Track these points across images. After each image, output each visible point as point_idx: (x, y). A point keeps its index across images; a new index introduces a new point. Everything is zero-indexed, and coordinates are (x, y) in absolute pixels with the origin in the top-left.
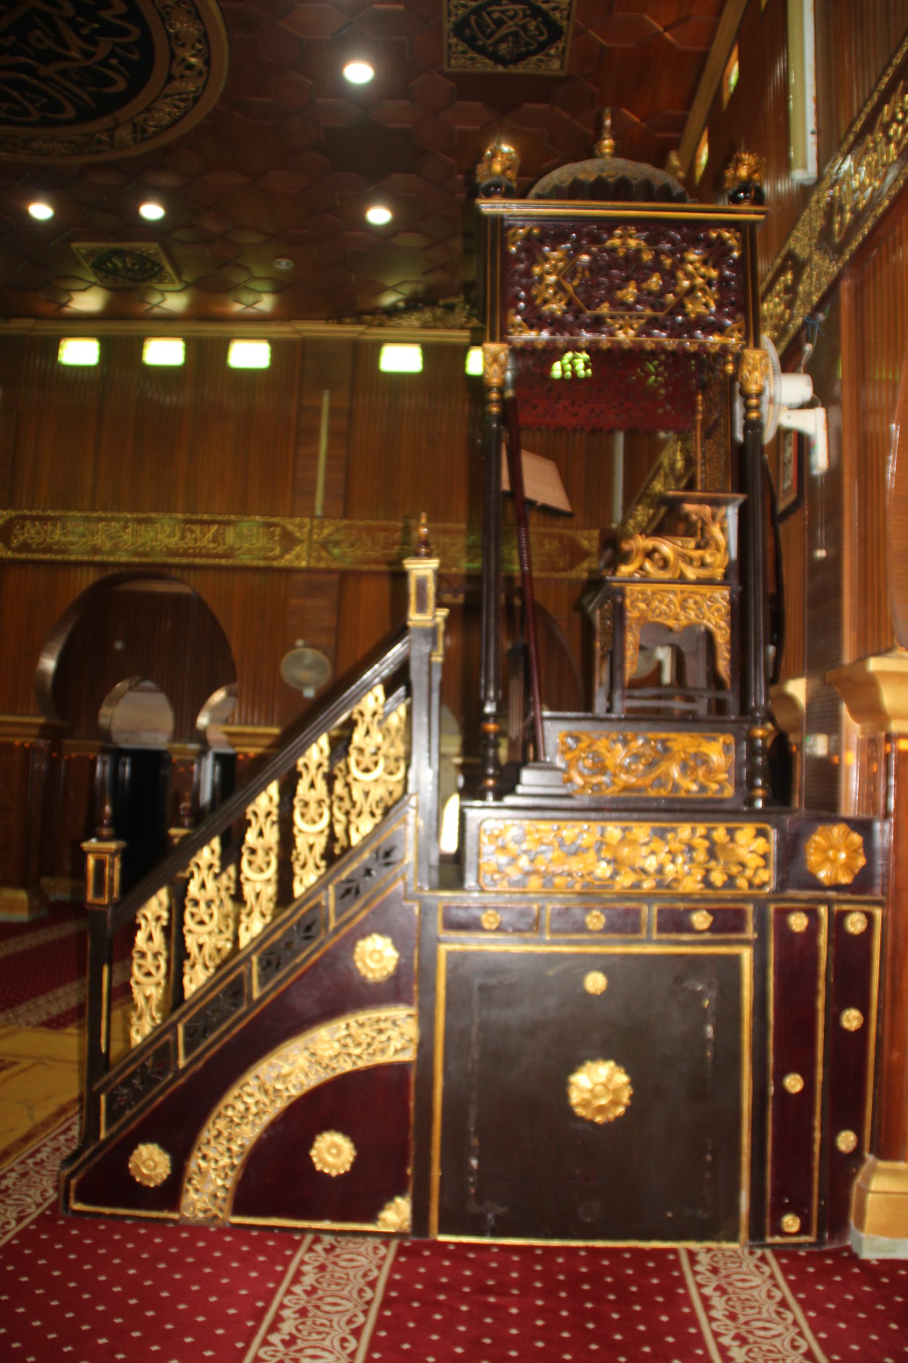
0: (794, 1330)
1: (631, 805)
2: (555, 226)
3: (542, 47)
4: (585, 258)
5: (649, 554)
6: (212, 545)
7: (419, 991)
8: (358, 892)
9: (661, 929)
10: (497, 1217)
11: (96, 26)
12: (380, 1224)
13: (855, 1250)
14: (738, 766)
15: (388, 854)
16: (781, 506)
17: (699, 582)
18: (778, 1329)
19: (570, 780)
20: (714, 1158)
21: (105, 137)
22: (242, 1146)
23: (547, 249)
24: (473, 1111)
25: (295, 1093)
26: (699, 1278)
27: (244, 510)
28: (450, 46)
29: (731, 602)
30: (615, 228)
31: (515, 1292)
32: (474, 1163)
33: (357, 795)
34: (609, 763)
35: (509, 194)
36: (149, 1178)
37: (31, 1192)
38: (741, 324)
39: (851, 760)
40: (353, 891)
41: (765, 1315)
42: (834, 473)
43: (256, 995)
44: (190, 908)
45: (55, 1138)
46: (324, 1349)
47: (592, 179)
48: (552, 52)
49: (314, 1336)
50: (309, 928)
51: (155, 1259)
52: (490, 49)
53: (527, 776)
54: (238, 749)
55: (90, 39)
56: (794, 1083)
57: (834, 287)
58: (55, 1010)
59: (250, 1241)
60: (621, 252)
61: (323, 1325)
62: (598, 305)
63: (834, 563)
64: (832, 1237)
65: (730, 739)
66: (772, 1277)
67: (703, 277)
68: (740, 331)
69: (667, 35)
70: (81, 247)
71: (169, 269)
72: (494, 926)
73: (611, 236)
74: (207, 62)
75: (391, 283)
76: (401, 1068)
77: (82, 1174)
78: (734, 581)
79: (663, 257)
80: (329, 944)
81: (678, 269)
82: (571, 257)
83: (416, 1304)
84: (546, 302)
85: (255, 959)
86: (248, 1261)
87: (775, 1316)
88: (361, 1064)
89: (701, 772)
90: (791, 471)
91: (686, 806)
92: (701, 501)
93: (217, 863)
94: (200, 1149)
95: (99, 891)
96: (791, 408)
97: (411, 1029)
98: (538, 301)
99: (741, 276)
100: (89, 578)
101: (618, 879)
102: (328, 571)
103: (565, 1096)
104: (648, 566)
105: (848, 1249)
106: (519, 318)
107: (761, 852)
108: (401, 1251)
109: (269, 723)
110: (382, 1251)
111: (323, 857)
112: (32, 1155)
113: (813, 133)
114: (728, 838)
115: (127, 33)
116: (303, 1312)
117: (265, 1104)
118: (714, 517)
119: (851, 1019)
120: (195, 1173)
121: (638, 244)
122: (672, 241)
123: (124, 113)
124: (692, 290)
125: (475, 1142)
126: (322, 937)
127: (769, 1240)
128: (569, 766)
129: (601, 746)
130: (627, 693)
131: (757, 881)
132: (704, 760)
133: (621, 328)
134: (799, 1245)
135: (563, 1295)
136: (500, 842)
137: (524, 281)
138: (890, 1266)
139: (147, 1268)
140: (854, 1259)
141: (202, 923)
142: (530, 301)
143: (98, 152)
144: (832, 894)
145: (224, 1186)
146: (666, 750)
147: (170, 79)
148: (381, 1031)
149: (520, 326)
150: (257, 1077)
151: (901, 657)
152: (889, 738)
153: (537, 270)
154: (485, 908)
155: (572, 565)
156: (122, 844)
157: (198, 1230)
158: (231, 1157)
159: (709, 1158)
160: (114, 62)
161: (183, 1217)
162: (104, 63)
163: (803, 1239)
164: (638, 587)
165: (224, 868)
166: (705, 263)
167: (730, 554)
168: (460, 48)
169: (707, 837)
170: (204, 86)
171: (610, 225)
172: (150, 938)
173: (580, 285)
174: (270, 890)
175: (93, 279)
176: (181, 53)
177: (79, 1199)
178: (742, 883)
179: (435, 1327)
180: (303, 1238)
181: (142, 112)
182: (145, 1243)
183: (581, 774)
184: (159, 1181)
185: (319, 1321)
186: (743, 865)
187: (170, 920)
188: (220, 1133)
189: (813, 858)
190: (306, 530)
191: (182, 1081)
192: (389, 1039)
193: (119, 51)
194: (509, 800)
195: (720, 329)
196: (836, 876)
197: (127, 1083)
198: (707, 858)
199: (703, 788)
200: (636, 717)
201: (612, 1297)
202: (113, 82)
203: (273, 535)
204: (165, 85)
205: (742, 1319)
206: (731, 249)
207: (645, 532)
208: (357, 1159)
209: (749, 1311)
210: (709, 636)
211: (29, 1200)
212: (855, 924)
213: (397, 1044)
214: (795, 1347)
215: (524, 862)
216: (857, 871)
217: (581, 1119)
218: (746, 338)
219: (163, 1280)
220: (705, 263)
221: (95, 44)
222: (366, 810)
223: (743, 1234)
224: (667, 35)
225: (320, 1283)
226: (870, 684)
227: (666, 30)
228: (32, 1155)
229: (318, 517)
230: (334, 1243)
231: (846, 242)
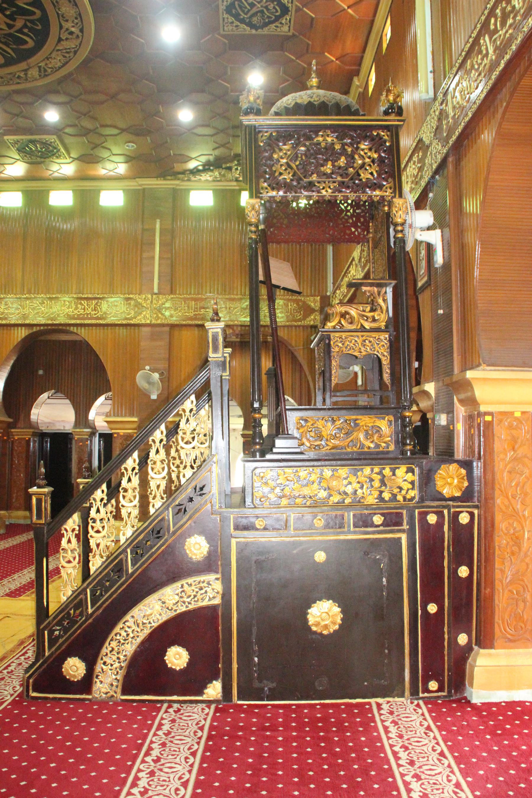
0: (434, 741)
1: (337, 457)
2: (285, 131)
3: (277, 18)
4: (303, 149)
5: (343, 315)
6: (94, 312)
7: (222, 564)
8: (185, 511)
9: (355, 526)
10: (270, 689)
11: (14, 9)
12: (204, 696)
13: (469, 698)
14: (397, 433)
15: (202, 489)
16: (420, 284)
17: (373, 330)
18: (426, 741)
19: (303, 444)
20: (389, 651)
21: (22, 75)
22: (125, 656)
23: (281, 144)
24: (254, 630)
25: (155, 625)
26: (382, 717)
27: (112, 291)
28: (224, 19)
29: (390, 341)
30: (320, 131)
31: (281, 729)
32: (256, 659)
33: (183, 457)
34: (324, 433)
35: (258, 113)
36: (75, 676)
37: (7, 688)
38: (392, 184)
39: (460, 427)
40: (183, 510)
41: (418, 735)
42: (447, 266)
43: (130, 571)
44: (91, 524)
45: (18, 658)
46: (176, 763)
47: (306, 103)
48: (284, 21)
49: (170, 757)
50: (159, 532)
51: (79, 721)
52: (247, 21)
53: (279, 443)
54: (113, 431)
55: (11, 17)
56: (432, 608)
57: (444, 161)
58: (13, 587)
59: (133, 708)
60: (323, 145)
61: (175, 751)
62: (311, 176)
63: (448, 316)
64: (456, 692)
65: (392, 418)
66: (423, 715)
67: (369, 157)
68: (390, 188)
69: (350, 11)
70: (10, 138)
71: (62, 150)
72: (262, 527)
73: (317, 135)
74: (82, 31)
75: (193, 155)
76: (214, 608)
77: (34, 677)
78: (391, 329)
79: (346, 147)
80: (170, 541)
81: (355, 153)
82: (295, 147)
83: (226, 738)
84: (281, 174)
85: (129, 551)
86: (132, 720)
87: (424, 735)
88: (191, 607)
89: (376, 437)
90: (424, 264)
91: (367, 457)
92: (372, 285)
93: (106, 498)
94: (102, 659)
95: (39, 516)
96: (422, 229)
97: (218, 586)
98: (277, 174)
99: (391, 157)
100: (22, 333)
101: (331, 498)
102: (163, 325)
103: (306, 620)
104: (343, 322)
105: (465, 698)
106: (265, 185)
107: (410, 480)
108: (217, 710)
109: (132, 415)
110: (207, 710)
111: (165, 492)
112: (6, 668)
113: (431, 72)
114: (391, 473)
115: (34, 13)
116: (164, 745)
117: (138, 632)
118: (379, 294)
119: (463, 572)
120: (100, 672)
121: (332, 140)
122: (352, 138)
123: (32, 61)
124: (362, 166)
125: (256, 648)
126: (166, 537)
127: (421, 695)
128: (301, 436)
129: (320, 424)
130: (332, 394)
131: (408, 497)
132: (378, 430)
133: (323, 188)
134: (439, 697)
135: (307, 729)
136: (264, 480)
137: (269, 162)
138: (488, 706)
139: (75, 726)
140: (468, 702)
141: (98, 532)
142: (272, 173)
143: (19, 83)
144: (451, 503)
145: (116, 679)
146: (356, 425)
147: (60, 40)
148: (201, 589)
149: (266, 188)
150: (133, 617)
151: (484, 370)
152: (480, 414)
153: (275, 156)
154: (257, 517)
155: (305, 317)
156: (51, 489)
157: (103, 704)
158: (119, 662)
159: (386, 651)
160: (26, 31)
161: (94, 697)
162: (20, 31)
163: (440, 694)
164: (337, 334)
165: (109, 500)
166: (370, 149)
167: (388, 314)
168: (230, 20)
169: (380, 473)
170: (80, 45)
171: (316, 129)
172: (69, 541)
173: (300, 164)
174: (135, 512)
175: (18, 157)
176: (66, 25)
177: (34, 690)
178: (400, 498)
179: (237, 749)
180: (162, 705)
181: (44, 60)
182: (73, 713)
183: (308, 440)
184: (80, 678)
185: (172, 749)
186: (401, 489)
187: (79, 530)
188: (113, 649)
189: (439, 483)
190: (149, 302)
191: (90, 621)
192: (206, 592)
193: (29, 24)
194: (268, 457)
195: (380, 187)
196: (452, 492)
197: (59, 623)
198: (380, 485)
199: (377, 446)
200: (336, 407)
201: (334, 729)
202: (26, 42)
203: (130, 304)
204: (57, 44)
205: (406, 737)
206: (385, 142)
207: (341, 303)
208: (190, 660)
209: (409, 733)
210: (380, 360)
211: (6, 693)
212: (464, 518)
213: (211, 594)
214: (434, 751)
215: (278, 490)
216: (463, 489)
217: (315, 633)
218: (394, 192)
219: (85, 731)
220: (370, 149)
221: (14, 20)
222: (188, 464)
223: (407, 693)
224: (350, 11)
225: (172, 729)
226: (467, 385)
227: (348, 7)
228: (6, 668)
229: (156, 294)
230: (180, 707)
231: (449, 136)
